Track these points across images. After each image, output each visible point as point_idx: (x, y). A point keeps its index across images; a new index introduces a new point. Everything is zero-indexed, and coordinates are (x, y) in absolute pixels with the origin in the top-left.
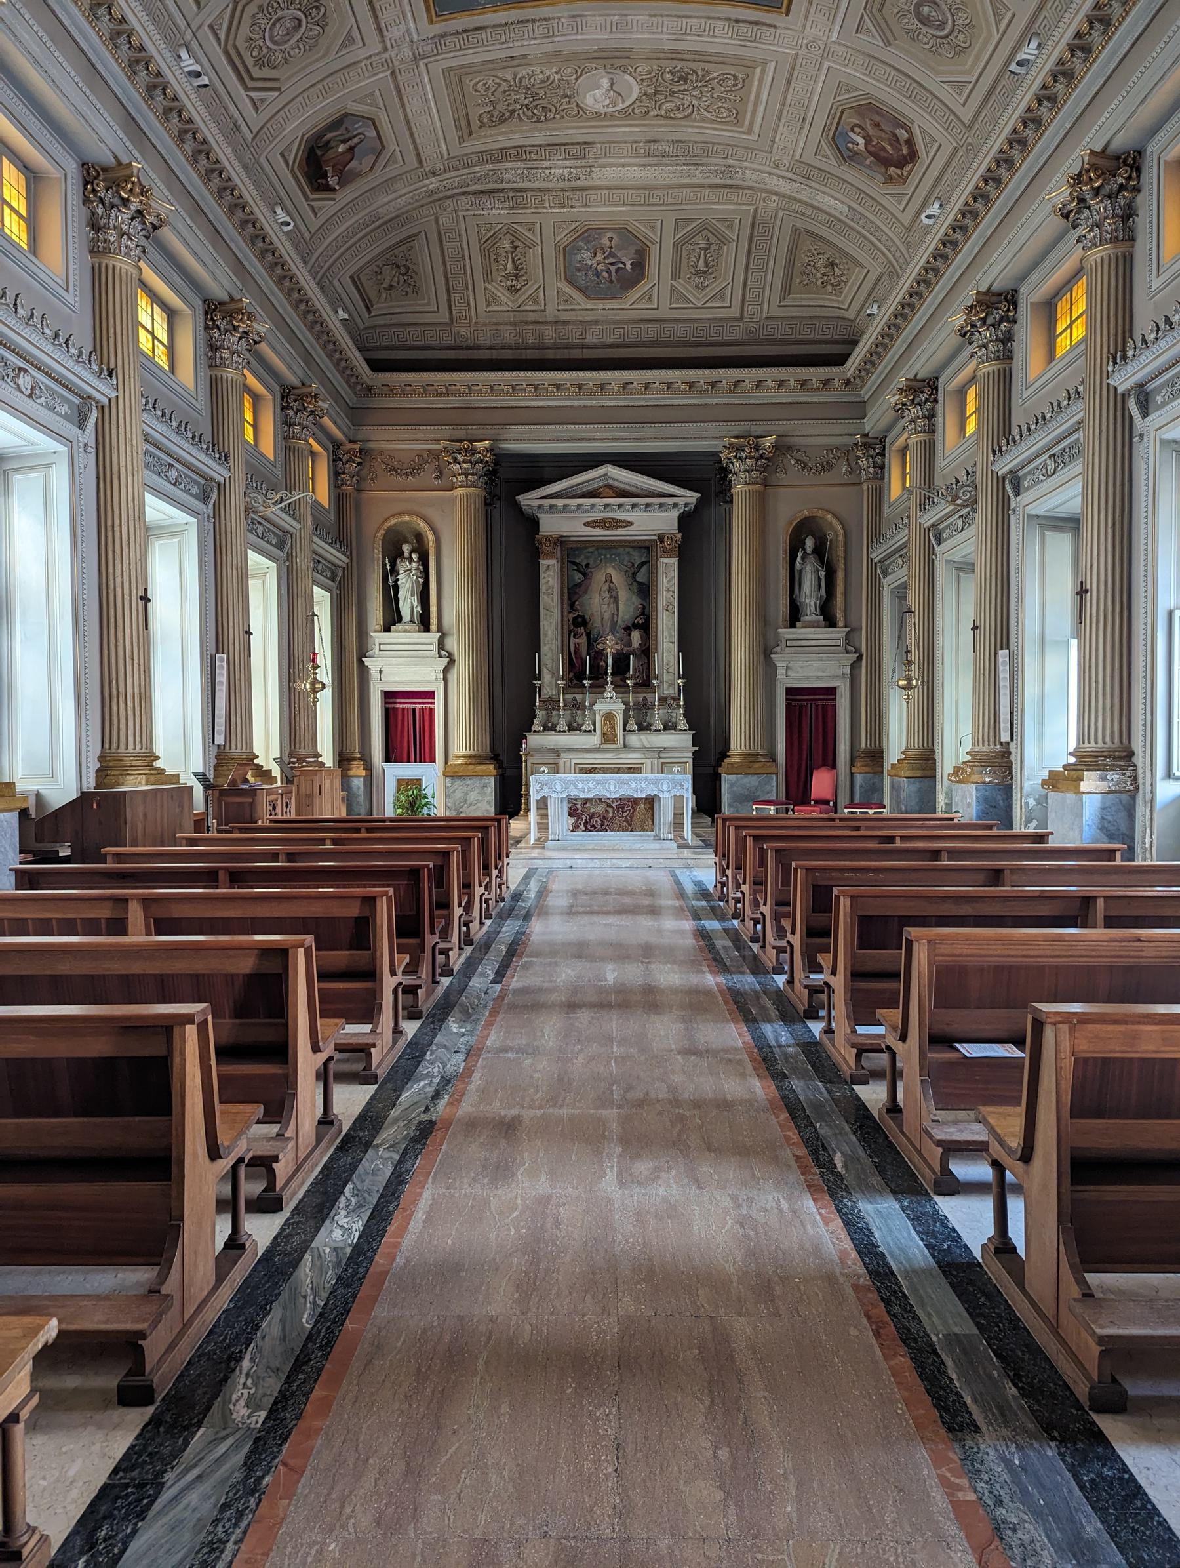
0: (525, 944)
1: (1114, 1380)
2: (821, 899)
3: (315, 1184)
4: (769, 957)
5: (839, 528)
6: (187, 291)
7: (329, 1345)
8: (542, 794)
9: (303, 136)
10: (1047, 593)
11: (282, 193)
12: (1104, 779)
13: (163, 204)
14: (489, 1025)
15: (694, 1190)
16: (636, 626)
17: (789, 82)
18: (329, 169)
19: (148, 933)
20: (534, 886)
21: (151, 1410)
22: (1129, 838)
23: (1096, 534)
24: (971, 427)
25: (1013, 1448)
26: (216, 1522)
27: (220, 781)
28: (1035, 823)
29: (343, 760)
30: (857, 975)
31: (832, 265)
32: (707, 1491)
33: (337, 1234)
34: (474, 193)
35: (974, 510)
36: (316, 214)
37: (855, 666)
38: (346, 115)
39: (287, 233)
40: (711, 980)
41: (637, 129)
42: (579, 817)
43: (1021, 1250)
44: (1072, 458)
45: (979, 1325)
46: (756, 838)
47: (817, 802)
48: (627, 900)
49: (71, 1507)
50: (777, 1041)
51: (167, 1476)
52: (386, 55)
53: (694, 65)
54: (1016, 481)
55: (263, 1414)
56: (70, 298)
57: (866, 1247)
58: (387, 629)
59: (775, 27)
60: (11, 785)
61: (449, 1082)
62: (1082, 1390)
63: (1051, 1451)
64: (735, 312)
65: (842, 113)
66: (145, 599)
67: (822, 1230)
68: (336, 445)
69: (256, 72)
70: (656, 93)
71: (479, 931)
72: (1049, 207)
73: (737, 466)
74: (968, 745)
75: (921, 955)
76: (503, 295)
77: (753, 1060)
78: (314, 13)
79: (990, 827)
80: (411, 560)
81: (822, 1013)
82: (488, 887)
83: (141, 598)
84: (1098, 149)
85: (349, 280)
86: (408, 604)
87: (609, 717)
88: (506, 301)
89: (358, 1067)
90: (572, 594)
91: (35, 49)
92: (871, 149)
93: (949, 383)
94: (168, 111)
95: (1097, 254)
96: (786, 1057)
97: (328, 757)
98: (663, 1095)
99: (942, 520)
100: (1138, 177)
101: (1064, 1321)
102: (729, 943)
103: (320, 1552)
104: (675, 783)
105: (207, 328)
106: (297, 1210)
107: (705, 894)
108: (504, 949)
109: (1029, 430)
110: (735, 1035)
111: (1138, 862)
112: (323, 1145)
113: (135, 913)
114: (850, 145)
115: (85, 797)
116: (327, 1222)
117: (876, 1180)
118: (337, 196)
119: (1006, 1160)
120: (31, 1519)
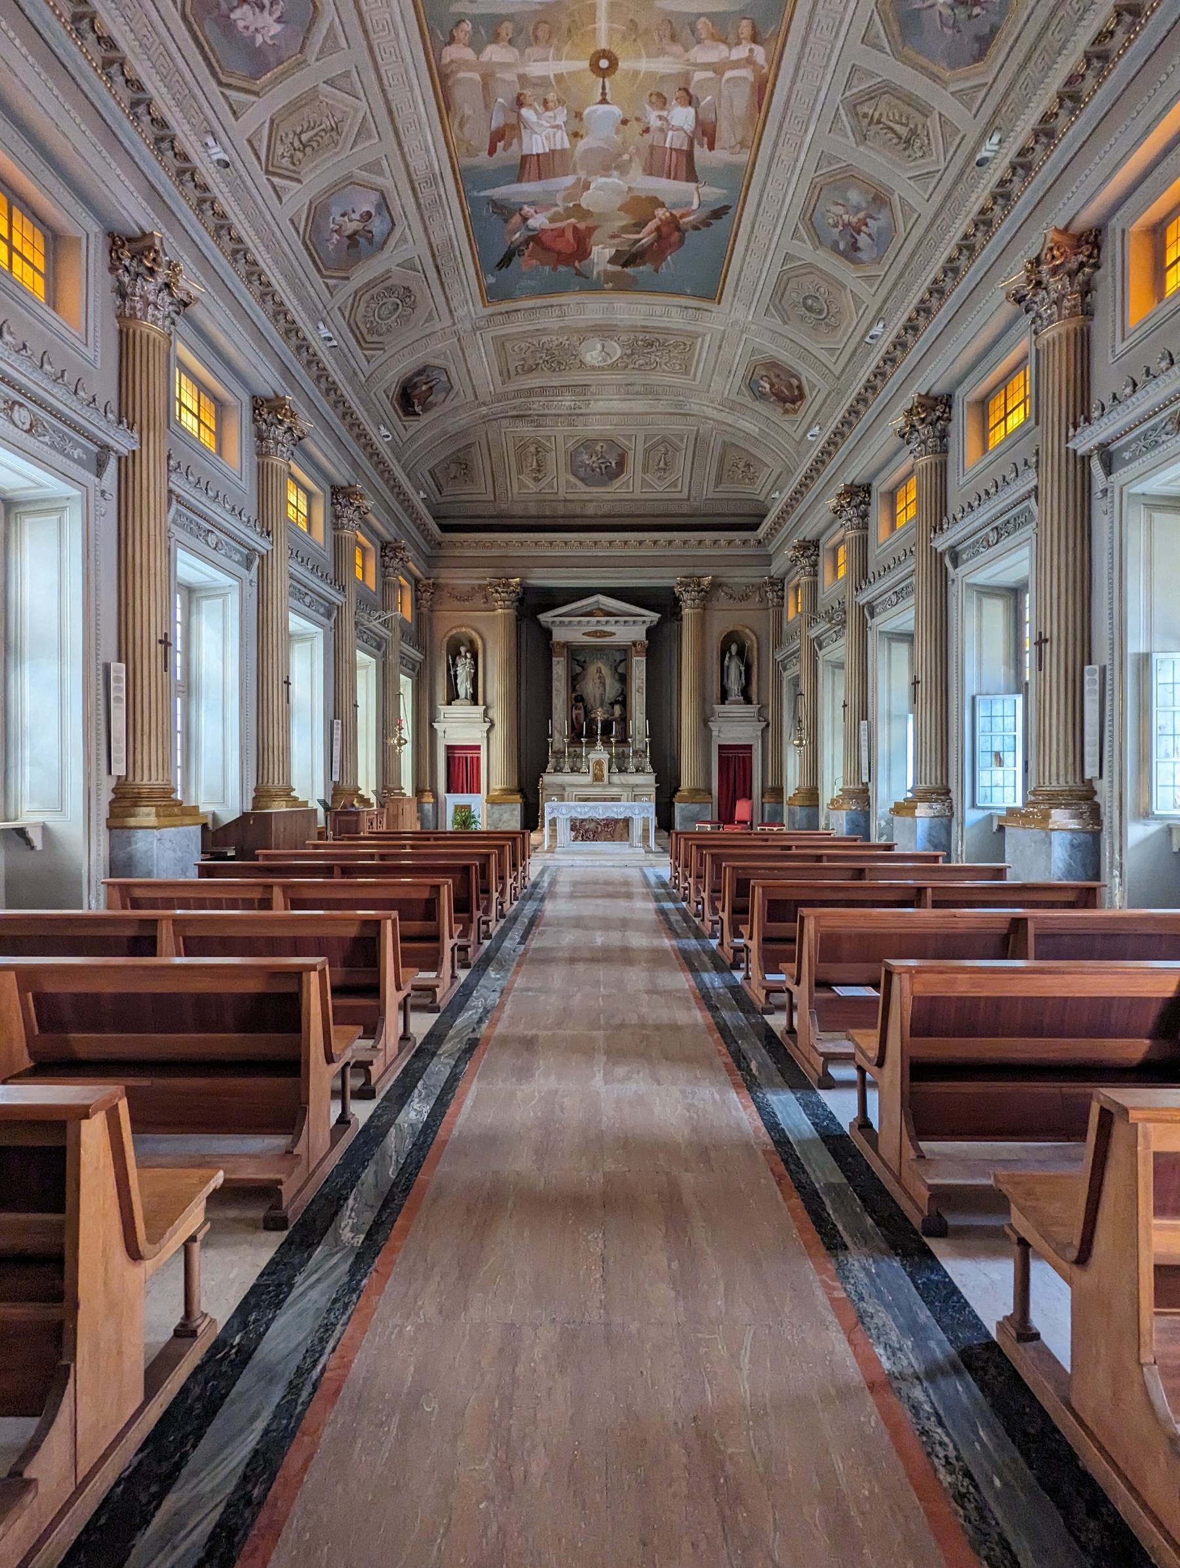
0: (541, 917)
1: (939, 1215)
2: (742, 888)
3: (398, 1080)
4: (707, 927)
5: (754, 638)
6: (321, 481)
7: (407, 1189)
8: (553, 815)
9: (311, 203)
10: (893, 682)
11: (385, 417)
12: (931, 808)
13: (306, 423)
14: (516, 973)
15: (655, 1086)
16: (617, 702)
18: (416, 401)
19: (286, 909)
20: (546, 879)
21: (286, 1233)
22: (947, 847)
23: (924, 645)
24: (842, 572)
25: (871, 1261)
26: (329, 1311)
27: (336, 805)
28: (885, 837)
29: (419, 791)
30: (766, 940)
31: (748, 465)
32: (663, 1291)
33: (412, 1115)
34: (512, 417)
35: (844, 627)
36: (280, 198)
37: (764, 731)
39: (387, 443)
40: (667, 943)
42: (578, 831)
43: (876, 1126)
44: (1027, 522)
45: (848, 1178)
46: (698, 847)
47: (740, 822)
48: (610, 889)
49: (231, 1301)
50: (712, 984)
51: (296, 1279)
53: (656, 336)
54: (871, 609)
55: (362, 1237)
56: (89, 353)
57: (772, 1125)
58: (449, 703)
60: (196, 808)
61: (488, 1011)
62: (917, 1221)
63: (896, 1263)
64: (684, 495)
65: (789, 279)
66: (287, 683)
67: (743, 1114)
68: (417, 581)
69: (368, 338)
71: (509, 909)
72: (891, 430)
73: (686, 596)
74: (840, 784)
75: (810, 927)
76: (530, 483)
77: (695, 997)
78: (407, 300)
79: (855, 840)
80: (466, 657)
81: (742, 966)
82: (515, 879)
83: (161, 642)
84: (923, 393)
85: (288, 222)
86: (464, 687)
87: (599, 763)
88: (532, 487)
89: (427, 1001)
90: (574, 680)
91: (222, 321)
93: (827, 543)
94: (309, 363)
95: (924, 461)
96: (718, 995)
97: (408, 790)
98: (635, 1021)
99: (822, 634)
101: (904, 1174)
102: (679, 918)
103: (400, 1331)
104: (643, 809)
105: (333, 504)
106: (385, 1099)
107: (664, 885)
108: (526, 921)
109: (987, 493)
110: (683, 981)
111: (953, 864)
112: (403, 1054)
113: (277, 894)
115: (245, 816)
116: (406, 1107)
117: (779, 1079)
118: (421, 419)
119: (866, 1065)
120: (204, 1307)
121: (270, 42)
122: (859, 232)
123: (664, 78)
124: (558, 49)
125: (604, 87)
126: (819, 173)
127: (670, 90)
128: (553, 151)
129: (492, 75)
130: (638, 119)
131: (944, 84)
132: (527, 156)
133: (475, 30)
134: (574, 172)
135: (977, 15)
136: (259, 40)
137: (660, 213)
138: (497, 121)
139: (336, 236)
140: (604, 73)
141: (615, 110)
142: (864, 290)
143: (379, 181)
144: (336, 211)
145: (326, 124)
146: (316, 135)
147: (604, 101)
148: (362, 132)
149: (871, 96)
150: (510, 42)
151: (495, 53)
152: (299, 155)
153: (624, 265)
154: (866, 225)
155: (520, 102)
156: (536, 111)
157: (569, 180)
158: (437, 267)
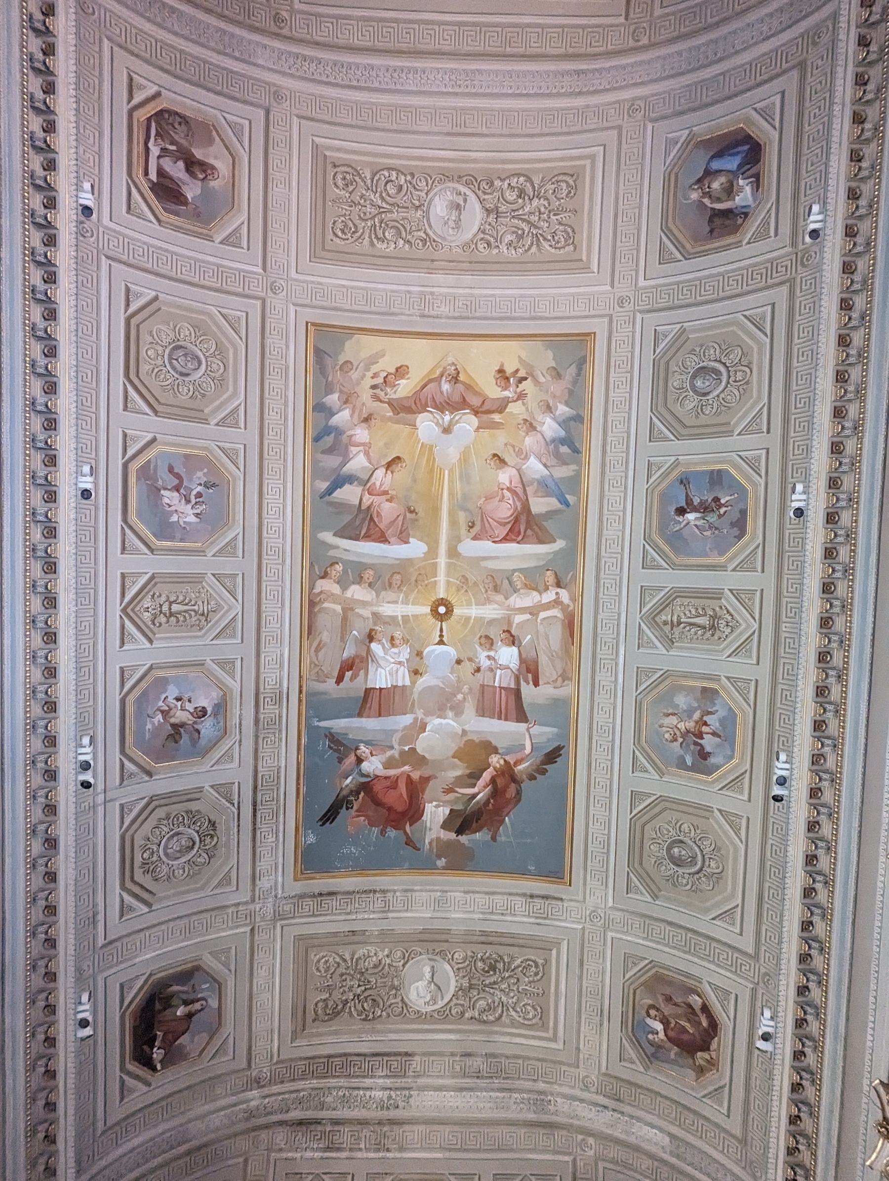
9: (151, 975)
36: (123, 643)
38: (197, 968)
41: (452, 1037)
52: (251, 907)
53: (502, 950)
59: (561, 899)
70: (471, 987)
78: (208, 840)
85: (118, 985)
92: (671, 1034)
114: (650, 1036)
121: (182, 523)
122: (700, 736)
123: (492, 622)
124: (407, 596)
125: (441, 630)
126: (640, 689)
127: (495, 633)
129: (352, 609)
130: (470, 660)
131: (723, 567)
133: (345, 571)
134: (412, 711)
136: (175, 518)
137: (496, 761)
138: (349, 652)
139: (159, 717)
140: (441, 618)
141: (450, 651)
142: (734, 802)
143: (228, 680)
144: (172, 692)
145: (200, 607)
146: (185, 611)
147: (441, 642)
148: (227, 631)
149: (666, 604)
150: (370, 585)
151: (357, 592)
152: (163, 619)
153: (460, 831)
154: (705, 724)
155: (371, 637)
156: (384, 647)
157: (407, 720)
158: (255, 804)
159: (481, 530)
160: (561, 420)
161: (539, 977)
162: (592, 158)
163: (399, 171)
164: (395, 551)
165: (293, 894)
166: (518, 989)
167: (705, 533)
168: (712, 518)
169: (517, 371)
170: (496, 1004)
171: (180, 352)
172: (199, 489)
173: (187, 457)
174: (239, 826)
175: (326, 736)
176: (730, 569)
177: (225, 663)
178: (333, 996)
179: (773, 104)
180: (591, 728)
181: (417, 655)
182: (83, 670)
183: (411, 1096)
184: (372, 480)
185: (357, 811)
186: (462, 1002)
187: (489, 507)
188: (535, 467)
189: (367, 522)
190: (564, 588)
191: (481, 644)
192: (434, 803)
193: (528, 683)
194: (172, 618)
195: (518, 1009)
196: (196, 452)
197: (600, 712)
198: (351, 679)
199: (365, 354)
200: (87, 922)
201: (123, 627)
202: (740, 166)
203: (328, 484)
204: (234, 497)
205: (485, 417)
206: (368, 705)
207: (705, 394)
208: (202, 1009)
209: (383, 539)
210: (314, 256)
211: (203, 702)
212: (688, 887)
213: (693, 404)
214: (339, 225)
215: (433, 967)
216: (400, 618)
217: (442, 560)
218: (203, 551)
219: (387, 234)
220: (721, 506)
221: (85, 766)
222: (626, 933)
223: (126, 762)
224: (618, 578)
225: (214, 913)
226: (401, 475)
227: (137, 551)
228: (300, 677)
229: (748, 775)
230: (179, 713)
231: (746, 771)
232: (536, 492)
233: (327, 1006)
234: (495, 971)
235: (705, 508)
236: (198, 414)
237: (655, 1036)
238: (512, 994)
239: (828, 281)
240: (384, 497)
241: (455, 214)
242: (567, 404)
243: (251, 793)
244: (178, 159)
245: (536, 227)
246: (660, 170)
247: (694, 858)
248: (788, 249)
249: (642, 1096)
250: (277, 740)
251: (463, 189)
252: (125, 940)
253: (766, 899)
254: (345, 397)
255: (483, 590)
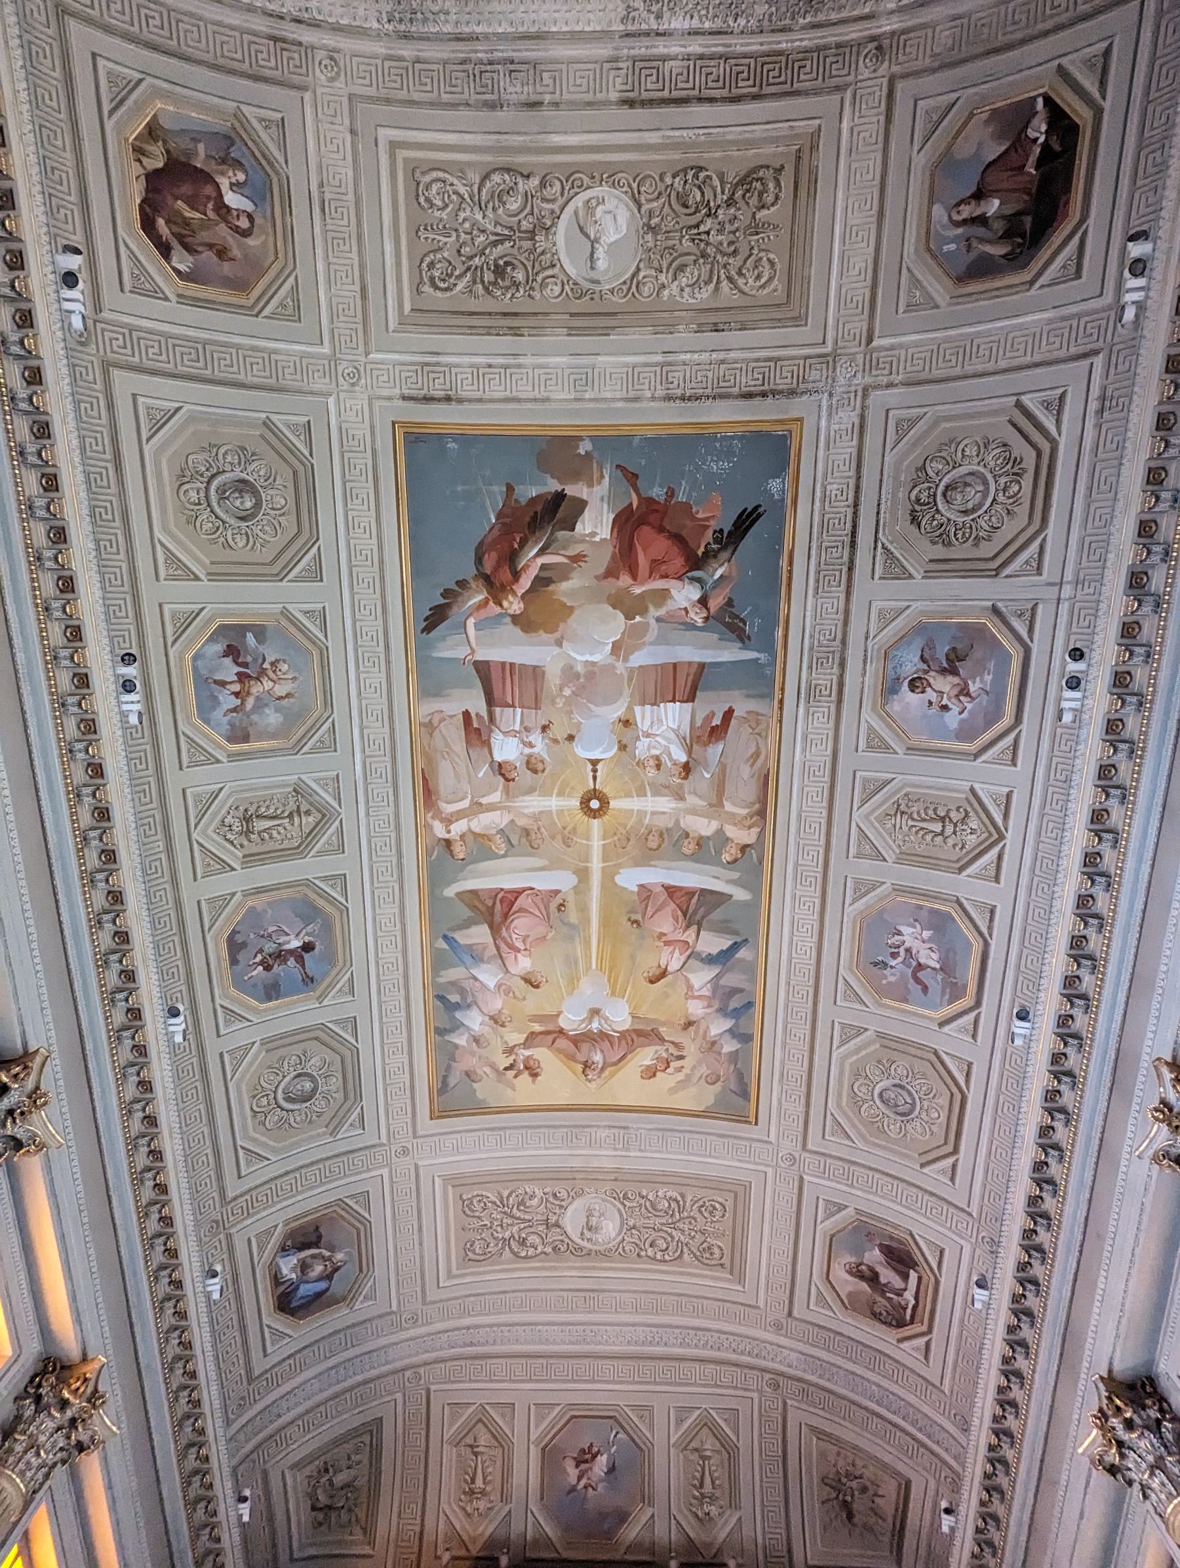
9: (1032, 283)
17: (363, 289)
36: (1009, 796)
38: (960, 280)
52: (868, 380)
53: (489, 305)
70: (532, 235)
78: (924, 497)
85: (1019, 762)
100: (1169, 1405)
122: (242, 677)
123: (530, 791)
124: (640, 821)
125: (595, 778)
128: (655, 703)
129: (711, 805)
130: (556, 741)
131: (246, 894)
132: (687, 701)
133: (719, 853)
134: (631, 671)
135: (255, 956)
137: (514, 605)
138: (715, 751)
139: (973, 688)
140: (595, 794)
142: (201, 779)
144: (952, 719)
145: (904, 823)
146: (924, 820)
147: (595, 763)
150: (687, 835)
151: (705, 827)
152: (954, 815)
153: (560, 497)
154: (237, 695)
155: (687, 768)
157: (639, 659)
158: (853, 544)
159: (549, 901)
160: (461, 1030)
161: (428, 260)
162: (450, 1275)
163: (654, 1259)
164: (656, 875)
165: (805, 397)
166: (458, 236)
167: (275, 928)
168: (270, 947)
169: (516, 1076)
170: (490, 205)
171: (901, 1109)
172: (893, 963)
173: (905, 1000)
174: (878, 513)
175: (749, 638)
176: (239, 894)
177: (879, 747)
178: (750, 215)
179: (273, 1344)
180: (388, 662)
181: (625, 747)
182: (1097, 557)
183: (624, 20)
184: (683, 958)
185: (707, 527)
186: (545, 205)
187: (541, 930)
188: (488, 976)
189: (690, 911)
190: (440, 839)
191: (542, 762)
192: (597, 539)
193: (477, 714)
194: (942, 814)
195: (454, 197)
196: (892, 1003)
197: (375, 634)
198: (713, 714)
199: (692, 1090)
200: (1114, 403)
201: (1006, 816)
202: (297, 1288)
203: (738, 955)
204: (852, 946)
205: (550, 1027)
206: (690, 678)
207: (299, 1075)
208: (958, 204)
209: (671, 891)
210: (747, 1187)
211: (913, 698)
212: (222, 451)
213: (312, 1062)
214: (718, 1214)
215: (592, 268)
216: (649, 794)
217: (596, 865)
218: (894, 890)
219: (667, 1205)
220: (261, 963)
221: (1074, 683)
222: (303, 356)
223: (1025, 635)
224: (374, 859)
225: (924, 375)
226: (649, 962)
227: (975, 904)
228: (781, 722)
229: (170, 640)
230: (946, 689)
231: (148, 440)
232: (485, 949)
233: (761, 194)
234: (496, 266)
235: (280, 956)
236: (886, 1042)
237: (233, 180)
238: (467, 225)
239: (153, 988)
240: (670, 938)
241: (594, 1221)
242: (456, 1046)
243: (858, 562)
244: (885, 1285)
245: (505, 1213)
246: (378, 1271)
247: (222, 498)
248: (233, 1231)
249: (239, 56)
250: (817, 636)
251: (584, 1244)
252: (1062, 354)
253: (71, 172)
254: (715, 1049)
255: (543, 830)
